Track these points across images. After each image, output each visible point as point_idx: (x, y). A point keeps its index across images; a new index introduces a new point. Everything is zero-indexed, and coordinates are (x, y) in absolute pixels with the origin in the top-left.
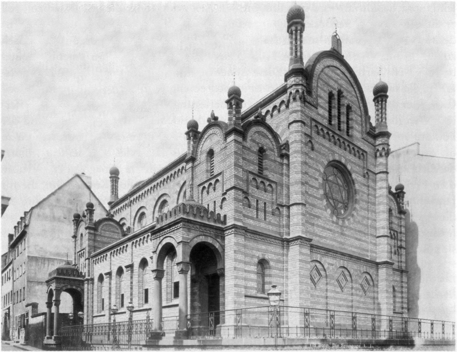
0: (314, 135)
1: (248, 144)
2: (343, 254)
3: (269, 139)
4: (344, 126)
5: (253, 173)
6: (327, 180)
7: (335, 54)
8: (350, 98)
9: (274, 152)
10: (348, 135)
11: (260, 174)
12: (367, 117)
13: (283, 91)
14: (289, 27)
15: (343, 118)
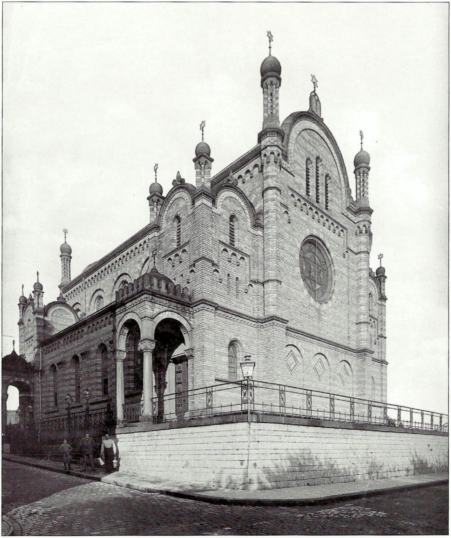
0: (291, 206)
1: (219, 210)
2: (320, 339)
3: (241, 206)
4: (322, 199)
5: (223, 243)
6: (304, 257)
7: (312, 115)
8: (329, 164)
9: (247, 221)
10: (327, 209)
11: (231, 245)
12: (349, 191)
13: (256, 153)
14: (263, 81)
15: (322, 190)
